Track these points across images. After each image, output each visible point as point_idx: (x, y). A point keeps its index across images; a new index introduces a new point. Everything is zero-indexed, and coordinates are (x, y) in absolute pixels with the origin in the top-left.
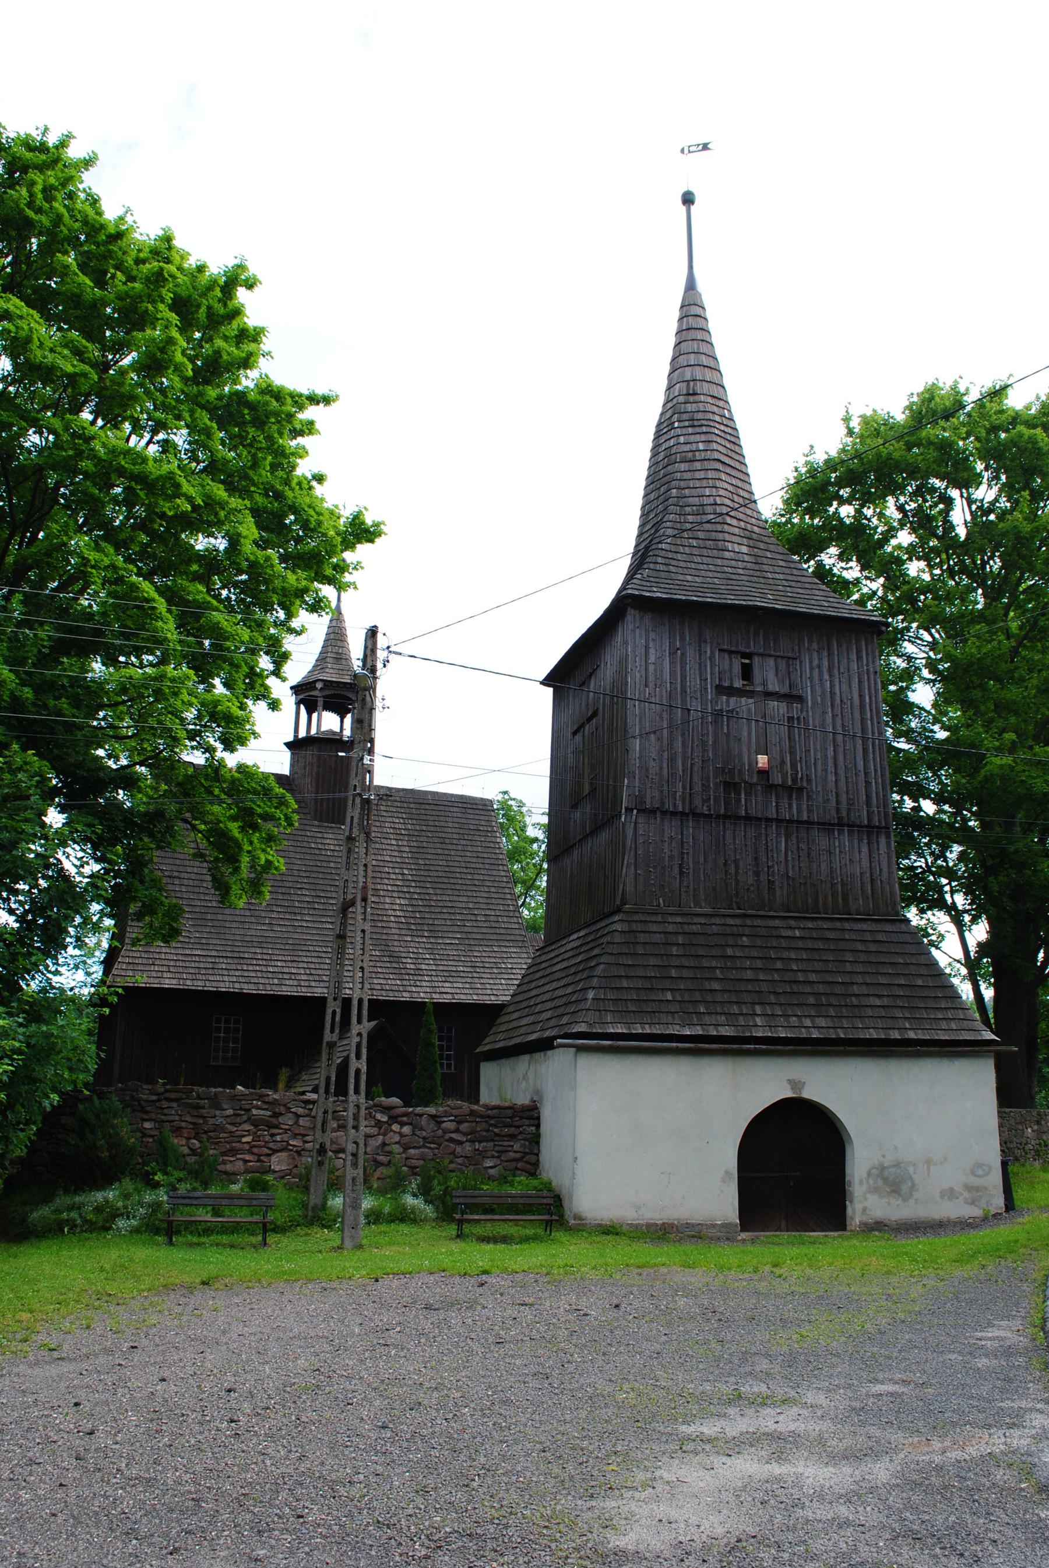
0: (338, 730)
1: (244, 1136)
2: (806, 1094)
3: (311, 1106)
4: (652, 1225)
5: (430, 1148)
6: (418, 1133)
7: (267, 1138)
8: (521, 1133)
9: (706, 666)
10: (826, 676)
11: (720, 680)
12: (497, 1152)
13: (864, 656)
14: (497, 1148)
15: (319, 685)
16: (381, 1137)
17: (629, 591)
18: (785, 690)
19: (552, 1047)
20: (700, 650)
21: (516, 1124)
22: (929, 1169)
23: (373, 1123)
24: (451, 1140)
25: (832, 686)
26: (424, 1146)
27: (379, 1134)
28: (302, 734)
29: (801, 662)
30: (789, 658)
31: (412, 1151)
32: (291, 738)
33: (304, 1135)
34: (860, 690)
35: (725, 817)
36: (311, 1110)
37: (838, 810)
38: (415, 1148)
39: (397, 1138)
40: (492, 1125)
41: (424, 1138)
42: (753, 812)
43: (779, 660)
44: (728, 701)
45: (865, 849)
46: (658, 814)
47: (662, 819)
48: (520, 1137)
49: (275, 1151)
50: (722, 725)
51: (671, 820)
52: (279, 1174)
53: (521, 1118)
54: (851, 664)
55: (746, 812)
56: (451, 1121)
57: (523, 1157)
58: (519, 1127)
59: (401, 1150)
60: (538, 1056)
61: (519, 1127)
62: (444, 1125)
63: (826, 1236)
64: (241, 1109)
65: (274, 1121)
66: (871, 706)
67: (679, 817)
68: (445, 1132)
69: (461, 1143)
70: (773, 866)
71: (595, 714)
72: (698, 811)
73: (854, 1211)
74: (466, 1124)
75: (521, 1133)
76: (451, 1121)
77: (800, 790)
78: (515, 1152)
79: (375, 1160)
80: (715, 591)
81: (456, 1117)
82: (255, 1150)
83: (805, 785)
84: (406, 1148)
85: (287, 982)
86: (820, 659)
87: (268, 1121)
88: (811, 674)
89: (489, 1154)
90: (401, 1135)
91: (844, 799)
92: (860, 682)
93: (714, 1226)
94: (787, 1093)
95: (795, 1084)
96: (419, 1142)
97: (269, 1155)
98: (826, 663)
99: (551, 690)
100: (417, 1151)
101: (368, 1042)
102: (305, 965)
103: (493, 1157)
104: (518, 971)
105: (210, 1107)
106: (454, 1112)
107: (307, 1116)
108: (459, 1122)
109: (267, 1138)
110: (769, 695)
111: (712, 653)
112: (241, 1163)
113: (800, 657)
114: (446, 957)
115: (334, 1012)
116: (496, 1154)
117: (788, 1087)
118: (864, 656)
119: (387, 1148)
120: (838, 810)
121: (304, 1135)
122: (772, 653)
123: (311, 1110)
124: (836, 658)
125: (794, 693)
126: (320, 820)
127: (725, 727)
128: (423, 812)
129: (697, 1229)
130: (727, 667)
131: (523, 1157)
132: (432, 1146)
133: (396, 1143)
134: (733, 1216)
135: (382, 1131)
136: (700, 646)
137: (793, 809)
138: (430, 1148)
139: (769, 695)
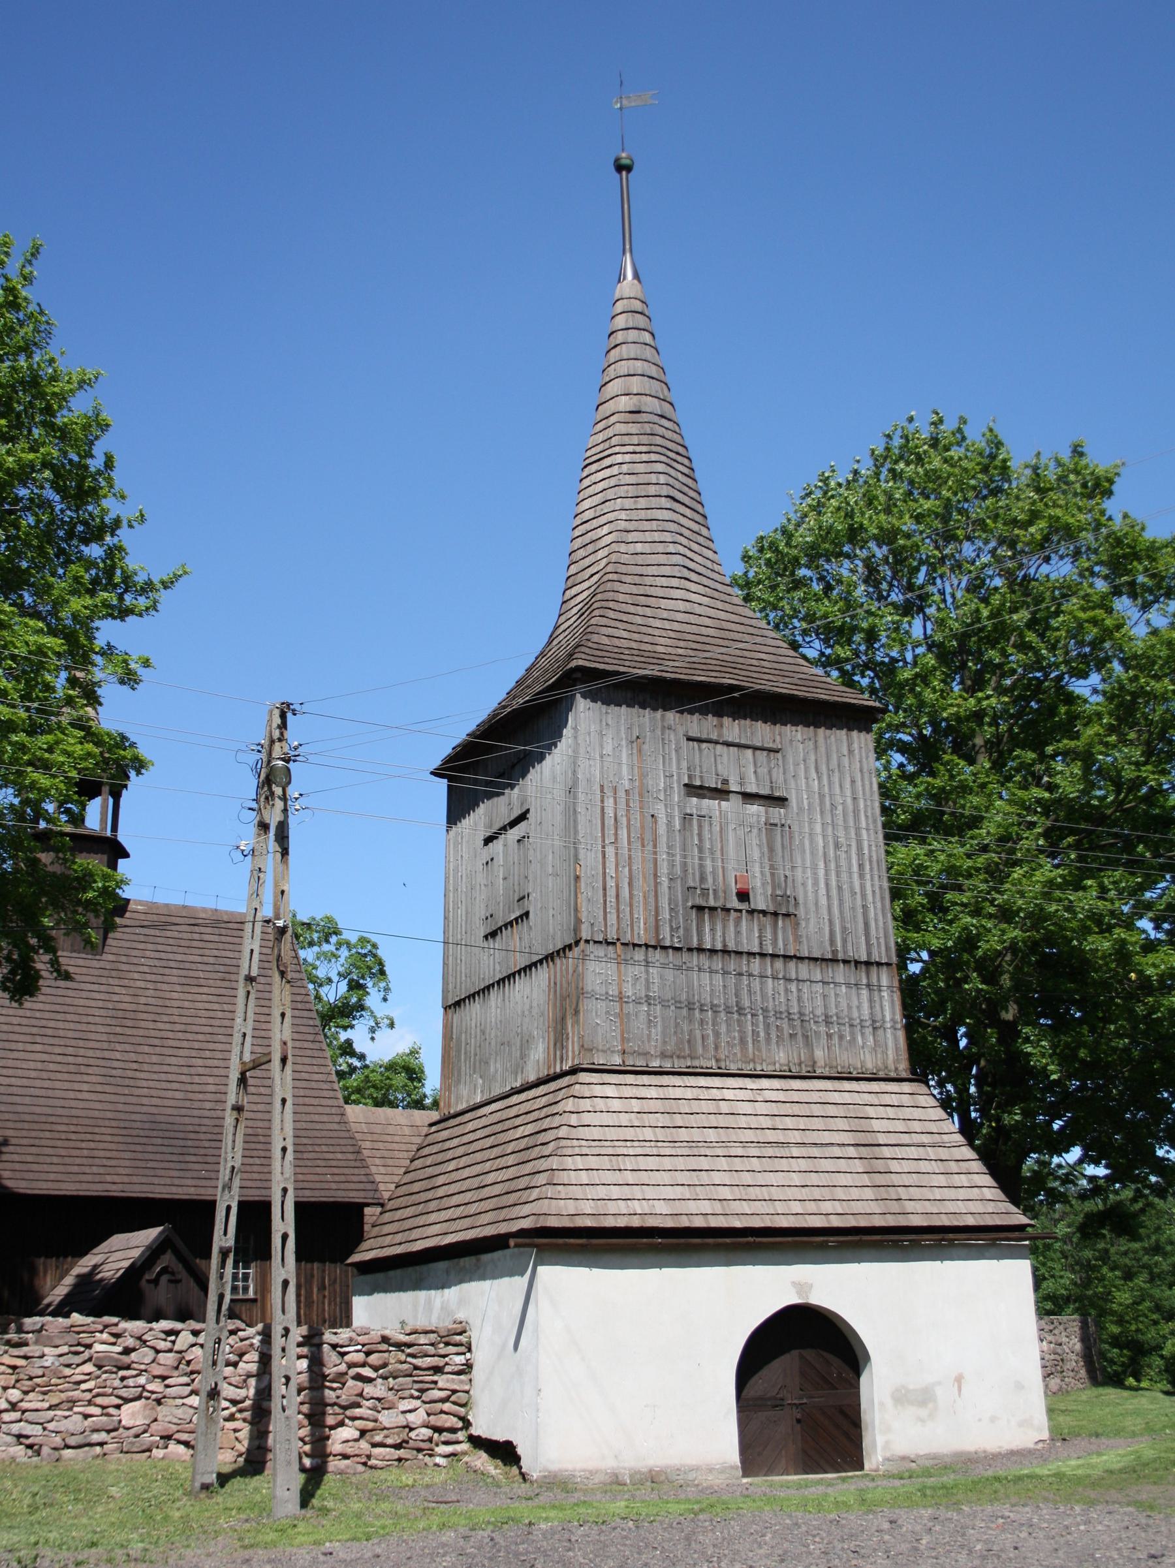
1: (84, 1381)
3: (173, 1338)
4: (636, 1473)
7: (117, 1383)
8: (447, 1364)
9: (670, 759)
10: (814, 775)
11: (690, 777)
12: (418, 1390)
17: (581, 663)
19: (507, 1246)
21: (442, 1352)
24: (359, 1377)
25: (821, 787)
34: (854, 792)
35: (831, 960)
37: (832, 941)
40: (409, 1355)
42: (731, 946)
43: (758, 752)
49: (127, 1401)
52: (132, 1431)
53: (447, 1344)
55: (725, 946)
57: (449, 1397)
58: (444, 1356)
60: (424, 1268)
61: (444, 1356)
62: (346, 1358)
63: (844, 1479)
64: (79, 1344)
65: (126, 1359)
66: (866, 812)
68: (351, 1365)
69: (369, 1380)
71: (522, 817)
73: (874, 1442)
75: (447, 1364)
80: (660, 659)
81: (363, 1345)
82: (99, 1400)
87: (117, 1360)
89: (406, 1393)
94: (793, 1299)
95: (800, 1287)
97: (118, 1407)
99: (444, 783)
101: (485, 1238)
103: (412, 1397)
104: (401, 1155)
105: (37, 1342)
106: (361, 1339)
107: (170, 1351)
108: (368, 1354)
109: (117, 1383)
112: (80, 1417)
116: (416, 1394)
117: (793, 1291)
120: (832, 941)
123: (173, 1342)
125: (777, 794)
126: (73, 951)
128: (196, 936)
131: (449, 1397)
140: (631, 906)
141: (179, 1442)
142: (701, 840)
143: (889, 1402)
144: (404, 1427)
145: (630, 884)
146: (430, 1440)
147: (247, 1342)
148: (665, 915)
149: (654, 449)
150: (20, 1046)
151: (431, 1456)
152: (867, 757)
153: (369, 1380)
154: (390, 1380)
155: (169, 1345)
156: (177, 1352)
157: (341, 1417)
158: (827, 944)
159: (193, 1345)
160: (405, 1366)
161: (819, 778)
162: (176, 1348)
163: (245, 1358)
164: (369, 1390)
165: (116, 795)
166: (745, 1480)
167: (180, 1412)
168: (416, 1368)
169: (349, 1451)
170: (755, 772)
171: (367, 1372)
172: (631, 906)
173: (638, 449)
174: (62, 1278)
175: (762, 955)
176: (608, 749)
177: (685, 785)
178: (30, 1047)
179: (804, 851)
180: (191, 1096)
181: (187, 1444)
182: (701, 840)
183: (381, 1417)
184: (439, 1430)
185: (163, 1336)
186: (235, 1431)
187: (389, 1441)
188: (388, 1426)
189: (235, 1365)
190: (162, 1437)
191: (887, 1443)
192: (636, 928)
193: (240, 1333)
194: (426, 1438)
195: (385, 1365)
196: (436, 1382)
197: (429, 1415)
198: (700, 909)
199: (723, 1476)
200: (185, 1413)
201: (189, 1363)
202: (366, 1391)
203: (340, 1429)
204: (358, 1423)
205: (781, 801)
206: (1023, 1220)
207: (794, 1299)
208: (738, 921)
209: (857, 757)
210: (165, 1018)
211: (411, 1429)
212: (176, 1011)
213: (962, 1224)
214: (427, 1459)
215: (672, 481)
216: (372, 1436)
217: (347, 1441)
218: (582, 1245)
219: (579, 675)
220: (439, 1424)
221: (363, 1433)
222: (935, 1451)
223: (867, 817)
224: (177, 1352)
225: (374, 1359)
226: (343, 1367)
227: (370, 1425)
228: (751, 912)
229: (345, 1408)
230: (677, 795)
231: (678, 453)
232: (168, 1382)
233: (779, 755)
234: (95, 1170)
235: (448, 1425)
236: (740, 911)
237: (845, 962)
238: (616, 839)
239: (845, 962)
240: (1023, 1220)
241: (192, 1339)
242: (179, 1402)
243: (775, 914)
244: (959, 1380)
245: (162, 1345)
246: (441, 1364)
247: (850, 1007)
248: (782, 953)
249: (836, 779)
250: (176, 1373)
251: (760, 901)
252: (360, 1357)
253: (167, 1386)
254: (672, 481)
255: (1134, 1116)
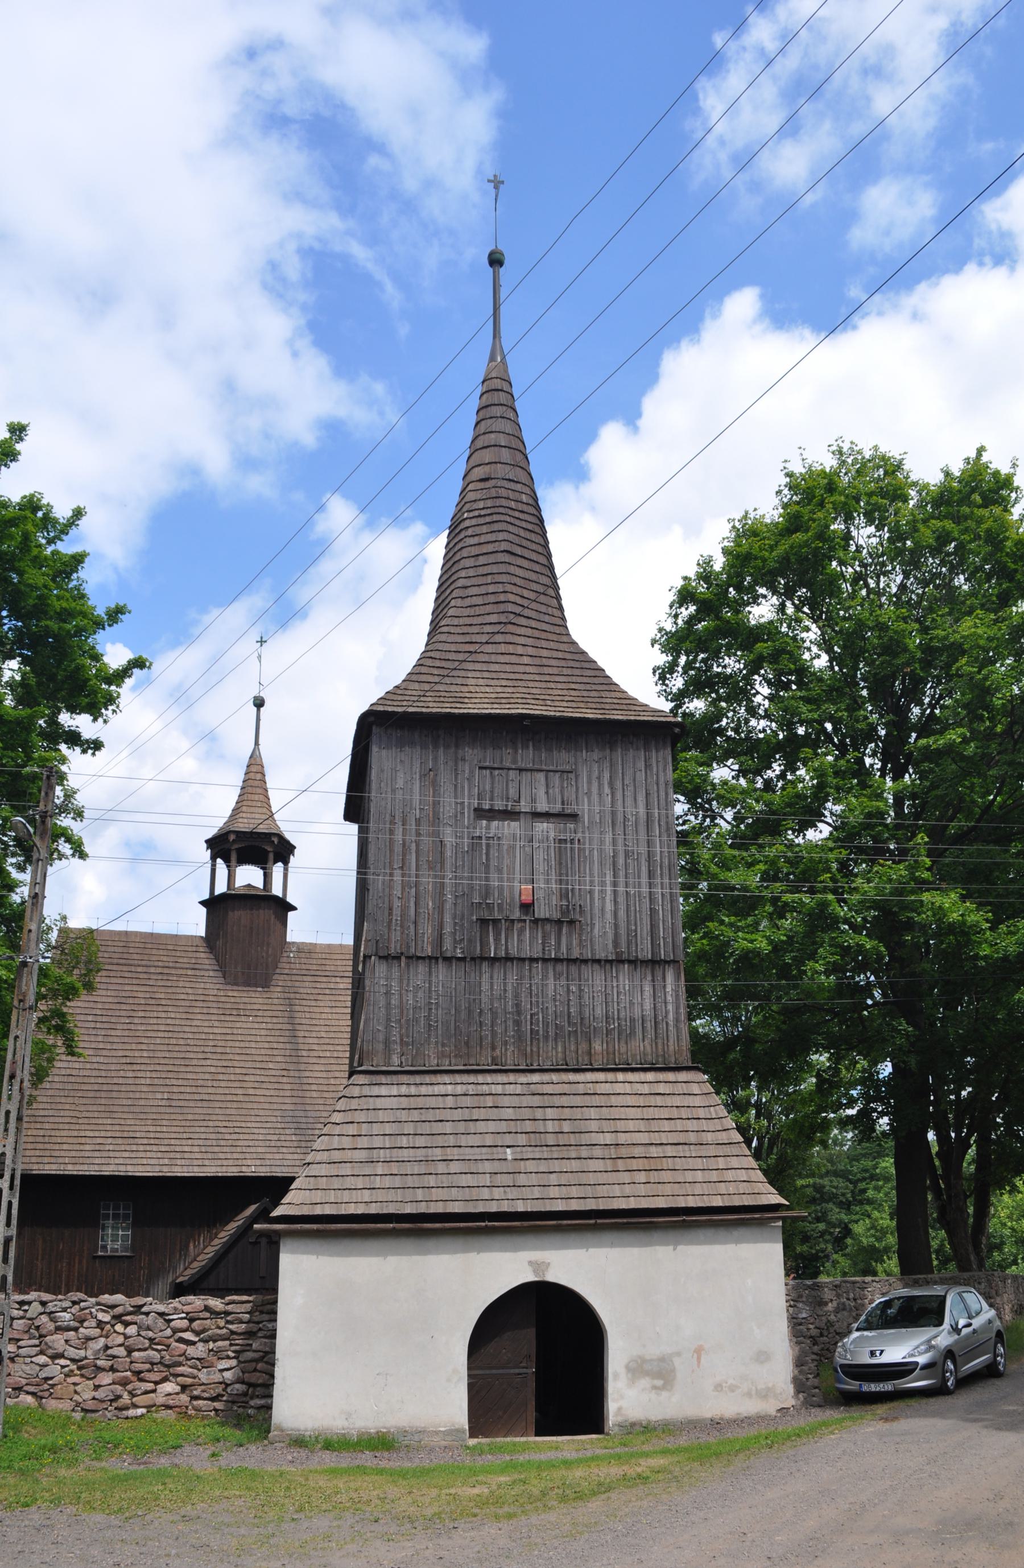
0: (261, 886)
2: (551, 1277)
3: (26, 1307)
5: (156, 1350)
6: (143, 1333)
9: (463, 787)
10: (607, 790)
12: (233, 1352)
13: (654, 765)
14: (233, 1348)
15: (232, 837)
16: (103, 1340)
18: (557, 808)
20: (456, 770)
22: (699, 1359)
23: (94, 1324)
26: (150, 1347)
27: (101, 1336)
28: (221, 888)
29: (577, 777)
30: (563, 772)
31: (136, 1354)
32: (206, 896)
33: (19, 1340)
36: (26, 1311)
37: (616, 943)
38: (139, 1350)
39: (120, 1339)
41: (151, 1340)
42: (514, 952)
44: (488, 828)
45: (648, 989)
46: (527, 963)
47: (408, 965)
48: (260, 1334)
50: (481, 855)
51: (417, 967)
54: (638, 774)
55: (507, 953)
56: (181, 1319)
57: (263, 1357)
58: (258, 1323)
59: (125, 1353)
61: (258, 1323)
62: (173, 1324)
67: (427, 961)
68: (175, 1331)
69: (193, 1343)
70: (538, 1014)
72: (449, 955)
74: (198, 1322)
75: (260, 1329)
76: (181, 1319)
77: (571, 922)
78: (255, 1351)
79: (95, 1366)
81: (187, 1314)
83: (578, 917)
84: (130, 1351)
85: (179, 1162)
86: (601, 772)
88: (589, 789)
90: (126, 1337)
91: (623, 931)
92: (647, 794)
93: (437, 1433)
96: (144, 1344)
98: (606, 775)
100: (142, 1354)
102: (201, 1142)
106: (187, 1308)
110: (537, 815)
111: (472, 772)
113: (575, 770)
114: (41, 1139)
115: (10, 1203)
116: (232, 1354)
118: (654, 765)
119: (109, 1352)
121: (19, 1340)
122: (544, 767)
123: (26, 1311)
124: (620, 767)
127: (484, 857)
129: (416, 1438)
130: (488, 787)
131: (263, 1357)
132: (159, 1347)
133: (120, 1345)
134: (462, 1419)
135: (104, 1333)
136: (456, 764)
137: (568, 945)
138: (156, 1350)
139: (537, 815)
140: (415, 923)
141: (28, 1393)
142: (488, 859)
143: (622, 1371)
144: (221, 1383)
145: (416, 904)
146: (245, 1394)
147: (87, 1311)
148: (448, 929)
149: (496, 510)
150: (195, 1062)
151: (244, 1407)
152: (665, 770)
153: (193, 1343)
154: (211, 1343)
155: (21, 1313)
156: (29, 1319)
157: (164, 1374)
158: (610, 946)
159: (41, 1314)
160: (225, 1331)
161: (613, 794)
162: (28, 1315)
163: (86, 1324)
164: (191, 1351)
165: (286, 862)
166: (472, 1442)
167: (27, 1368)
168: (233, 1332)
169: (171, 1402)
170: (547, 793)
171: (188, 1336)
172: (415, 923)
173: (483, 512)
174: (212, 1240)
175: (545, 960)
176: (400, 783)
177: (475, 810)
178: (204, 1063)
179: (592, 862)
180: (73, 1107)
181: (33, 1394)
182: (488, 859)
183: (201, 1375)
184: (250, 1385)
185: (17, 1306)
186: (75, 1384)
187: (206, 1395)
188: (205, 1382)
189: (76, 1329)
190: (14, 1389)
191: (620, 1409)
192: (420, 942)
193: (82, 1304)
194: (240, 1392)
195: (204, 1331)
196: (251, 1345)
197: (243, 1372)
198: (483, 922)
199: (449, 1438)
200: (31, 1369)
201: (38, 1328)
202: (188, 1352)
203: (165, 1384)
204: (179, 1379)
205: (574, 817)
206: (777, 1199)
207: (530, 1277)
208: (521, 931)
209: (655, 769)
210: (314, 1034)
211: (227, 1385)
212: (323, 1029)
213: (766, 1203)
214: (241, 1410)
215: (511, 537)
216: (191, 1391)
217: (170, 1394)
218: (318, 1231)
219: (372, 719)
220: (253, 1380)
221: (184, 1388)
222: (668, 1417)
223: (660, 825)
224: (29, 1319)
225: (196, 1325)
226: (169, 1332)
227: (189, 1381)
228: (536, 921)
229: (168, 1366)
230: (468, 817)
231: (522, 512)
232: (21, 1343)
233: (572, 776)
234: (235, 1156)
235: (260, 1381)
236: (525, 921)
237: (630, 962)
238: (403, 864)
239: (630, 962)
240: (777, 1199)
241: (40, 1309)
242: (28, 1360)
243: (559, 922)
244: (699, 1351)
245: (16, 1313)
246: (255, 1330)
247: (631, 1003)
248: (565, 957)
249: (628, 793)
250: (26, 1336)
251: (542, 911)
252: (185, 1323)
253: (19, 1347)
254: (511, 537)
255: (958, 1095)
